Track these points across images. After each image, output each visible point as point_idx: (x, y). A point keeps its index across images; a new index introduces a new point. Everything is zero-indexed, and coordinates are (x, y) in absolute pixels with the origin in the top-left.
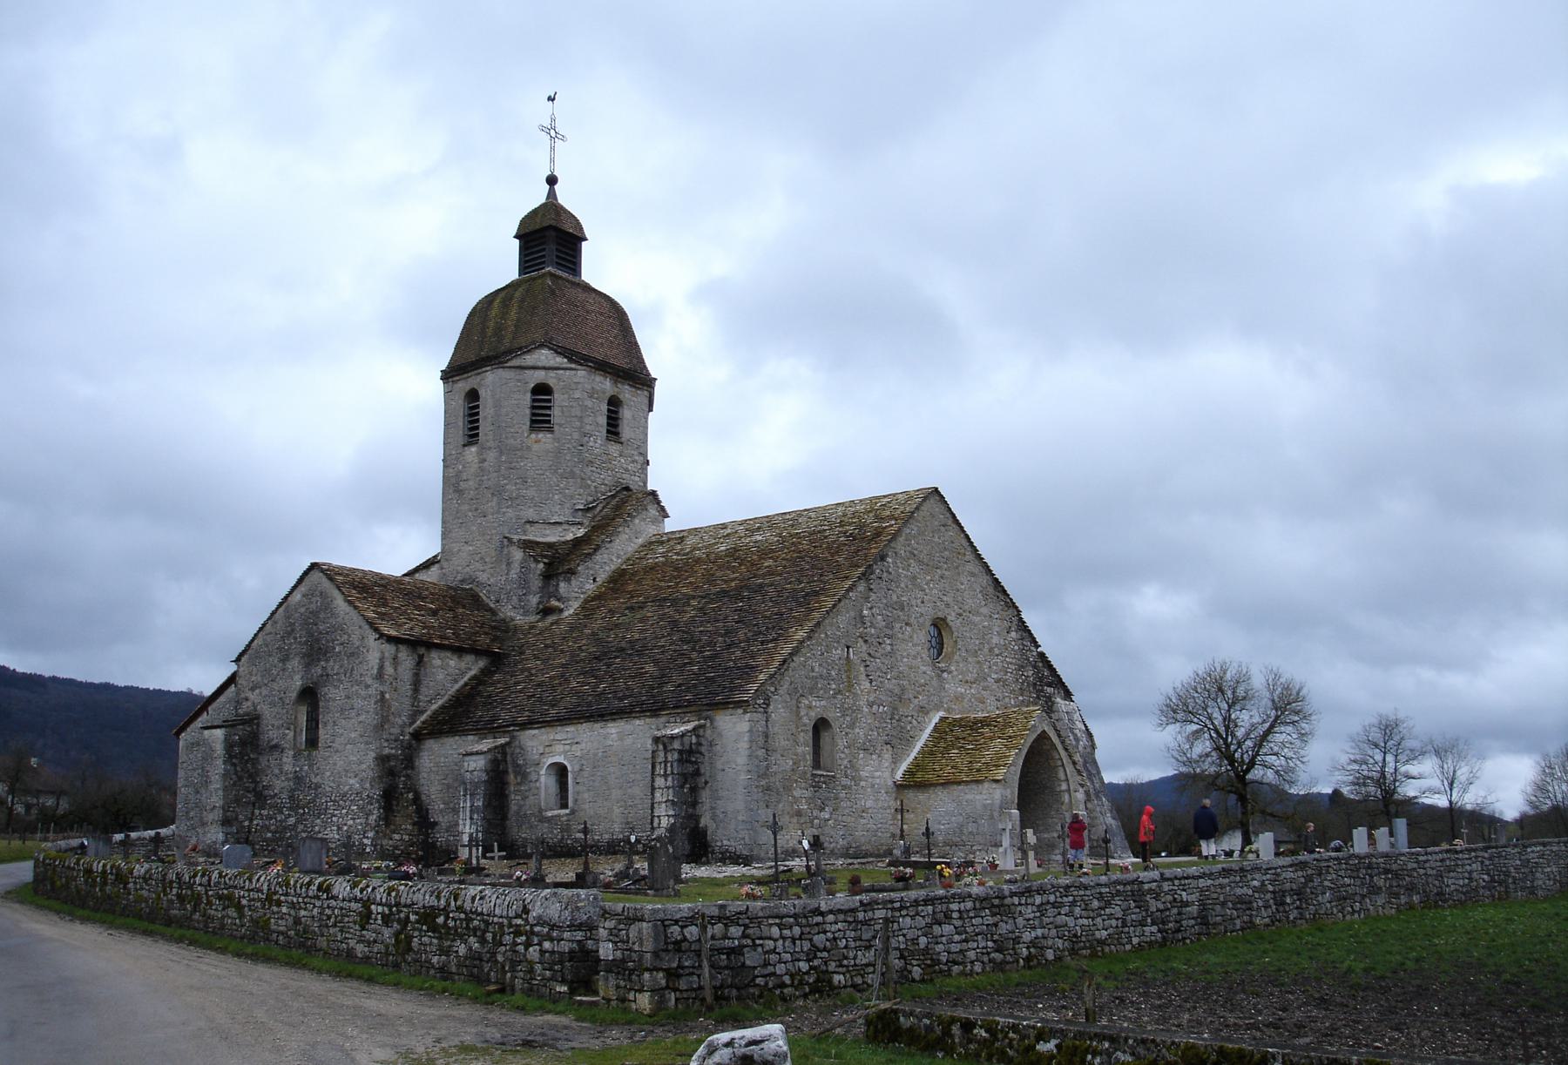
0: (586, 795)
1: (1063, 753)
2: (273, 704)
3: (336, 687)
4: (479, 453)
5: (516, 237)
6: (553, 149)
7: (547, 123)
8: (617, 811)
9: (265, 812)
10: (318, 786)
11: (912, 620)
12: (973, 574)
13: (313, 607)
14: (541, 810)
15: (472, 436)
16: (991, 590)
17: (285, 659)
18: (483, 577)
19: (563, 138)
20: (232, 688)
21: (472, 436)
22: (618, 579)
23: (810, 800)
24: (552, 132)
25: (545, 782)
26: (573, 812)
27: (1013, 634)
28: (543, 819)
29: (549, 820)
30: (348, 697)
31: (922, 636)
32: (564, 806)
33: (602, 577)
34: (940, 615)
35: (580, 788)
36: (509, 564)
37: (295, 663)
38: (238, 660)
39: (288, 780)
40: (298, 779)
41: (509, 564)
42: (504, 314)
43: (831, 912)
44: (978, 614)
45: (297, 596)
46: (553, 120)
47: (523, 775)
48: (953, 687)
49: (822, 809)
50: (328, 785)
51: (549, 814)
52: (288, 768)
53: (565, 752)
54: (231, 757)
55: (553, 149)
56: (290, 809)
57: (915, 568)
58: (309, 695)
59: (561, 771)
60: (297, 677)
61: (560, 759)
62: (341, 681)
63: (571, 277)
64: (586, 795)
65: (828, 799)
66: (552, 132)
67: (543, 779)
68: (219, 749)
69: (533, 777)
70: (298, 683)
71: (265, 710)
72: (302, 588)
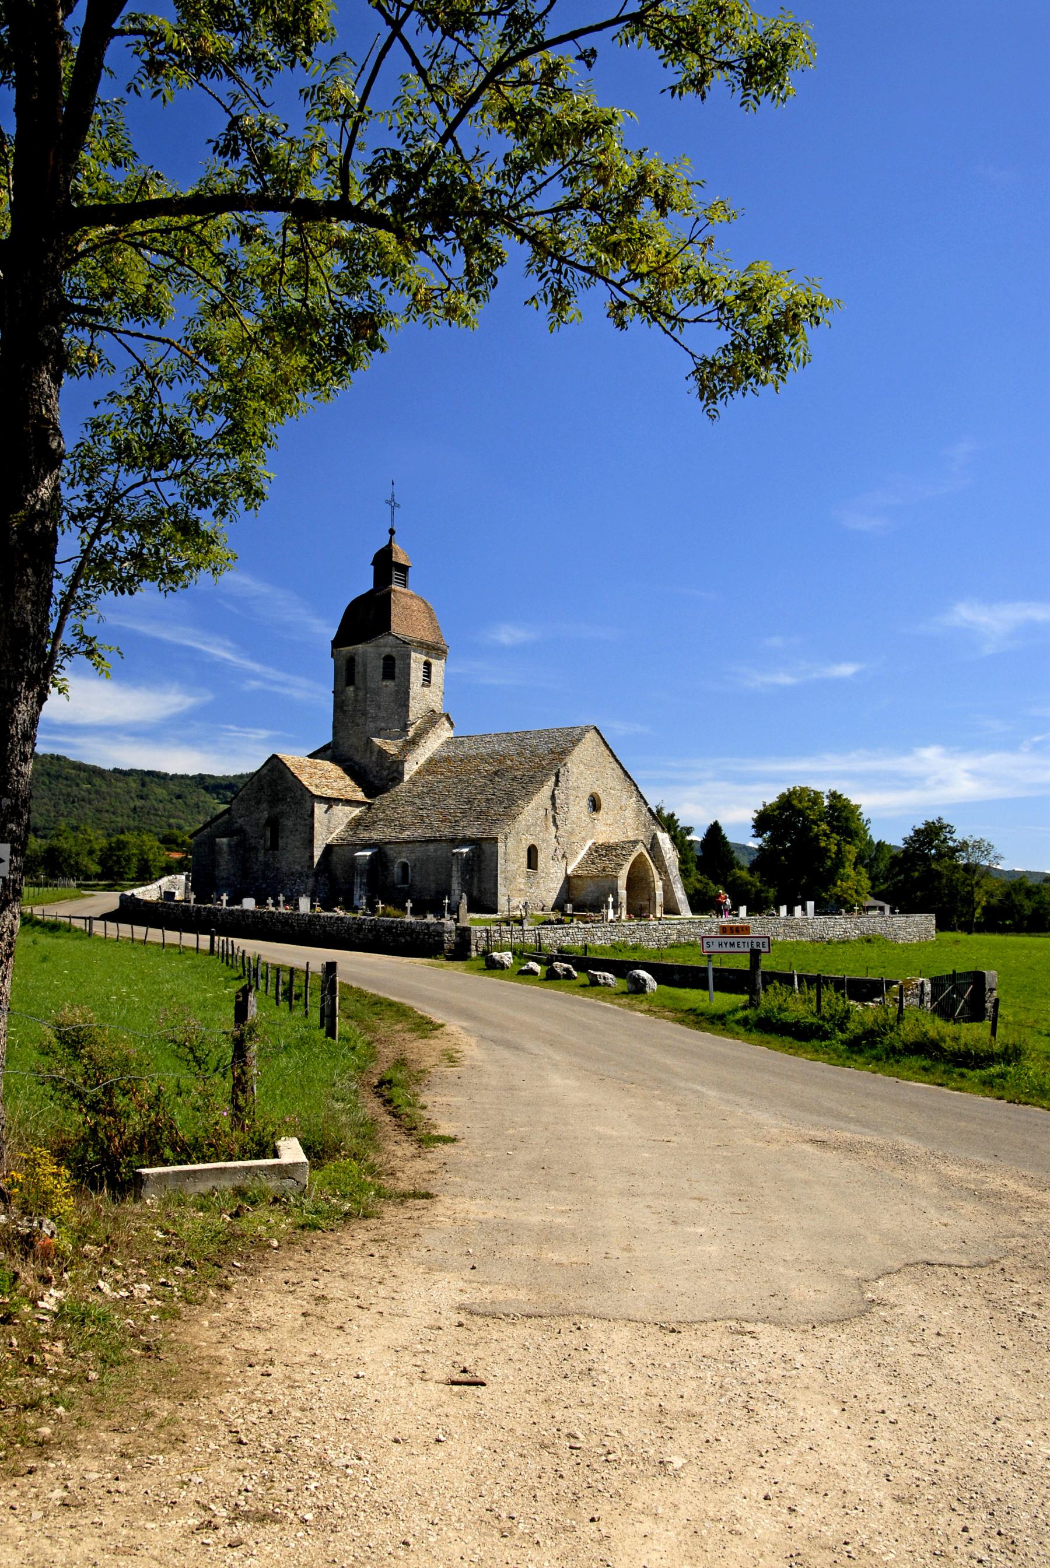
4: (355, 691)
6: (393, 513)
7: (389, 499)
8: (433, 886)
10: (278, 869)
14: (394, 885)
15: (350, 680)
16: (623, 776)
17: (258, 803)
18: (357, 758)
19: (399, 506)
20: (227, 816)
21: (350, 680)
22: (430, 761)
23: (525, 884)
24: (393, 504)
25: (396, 870)
26: (411, 885)
31: (585, 802)
33: (422, 761)
36: (371, 753)
37: (265, 805)
40: (266, 864)
41: (371, 753)
43: (901, 1010)
46: (393, 496)
48: (600, 827)
50: (285, 869)
55: (393, 513)
57: (582, 767)
58: (274, 824)
61: (403, 860)
63: (493, 916)
66: (393, 504)
68: (225, 848)
71: (247, 828)
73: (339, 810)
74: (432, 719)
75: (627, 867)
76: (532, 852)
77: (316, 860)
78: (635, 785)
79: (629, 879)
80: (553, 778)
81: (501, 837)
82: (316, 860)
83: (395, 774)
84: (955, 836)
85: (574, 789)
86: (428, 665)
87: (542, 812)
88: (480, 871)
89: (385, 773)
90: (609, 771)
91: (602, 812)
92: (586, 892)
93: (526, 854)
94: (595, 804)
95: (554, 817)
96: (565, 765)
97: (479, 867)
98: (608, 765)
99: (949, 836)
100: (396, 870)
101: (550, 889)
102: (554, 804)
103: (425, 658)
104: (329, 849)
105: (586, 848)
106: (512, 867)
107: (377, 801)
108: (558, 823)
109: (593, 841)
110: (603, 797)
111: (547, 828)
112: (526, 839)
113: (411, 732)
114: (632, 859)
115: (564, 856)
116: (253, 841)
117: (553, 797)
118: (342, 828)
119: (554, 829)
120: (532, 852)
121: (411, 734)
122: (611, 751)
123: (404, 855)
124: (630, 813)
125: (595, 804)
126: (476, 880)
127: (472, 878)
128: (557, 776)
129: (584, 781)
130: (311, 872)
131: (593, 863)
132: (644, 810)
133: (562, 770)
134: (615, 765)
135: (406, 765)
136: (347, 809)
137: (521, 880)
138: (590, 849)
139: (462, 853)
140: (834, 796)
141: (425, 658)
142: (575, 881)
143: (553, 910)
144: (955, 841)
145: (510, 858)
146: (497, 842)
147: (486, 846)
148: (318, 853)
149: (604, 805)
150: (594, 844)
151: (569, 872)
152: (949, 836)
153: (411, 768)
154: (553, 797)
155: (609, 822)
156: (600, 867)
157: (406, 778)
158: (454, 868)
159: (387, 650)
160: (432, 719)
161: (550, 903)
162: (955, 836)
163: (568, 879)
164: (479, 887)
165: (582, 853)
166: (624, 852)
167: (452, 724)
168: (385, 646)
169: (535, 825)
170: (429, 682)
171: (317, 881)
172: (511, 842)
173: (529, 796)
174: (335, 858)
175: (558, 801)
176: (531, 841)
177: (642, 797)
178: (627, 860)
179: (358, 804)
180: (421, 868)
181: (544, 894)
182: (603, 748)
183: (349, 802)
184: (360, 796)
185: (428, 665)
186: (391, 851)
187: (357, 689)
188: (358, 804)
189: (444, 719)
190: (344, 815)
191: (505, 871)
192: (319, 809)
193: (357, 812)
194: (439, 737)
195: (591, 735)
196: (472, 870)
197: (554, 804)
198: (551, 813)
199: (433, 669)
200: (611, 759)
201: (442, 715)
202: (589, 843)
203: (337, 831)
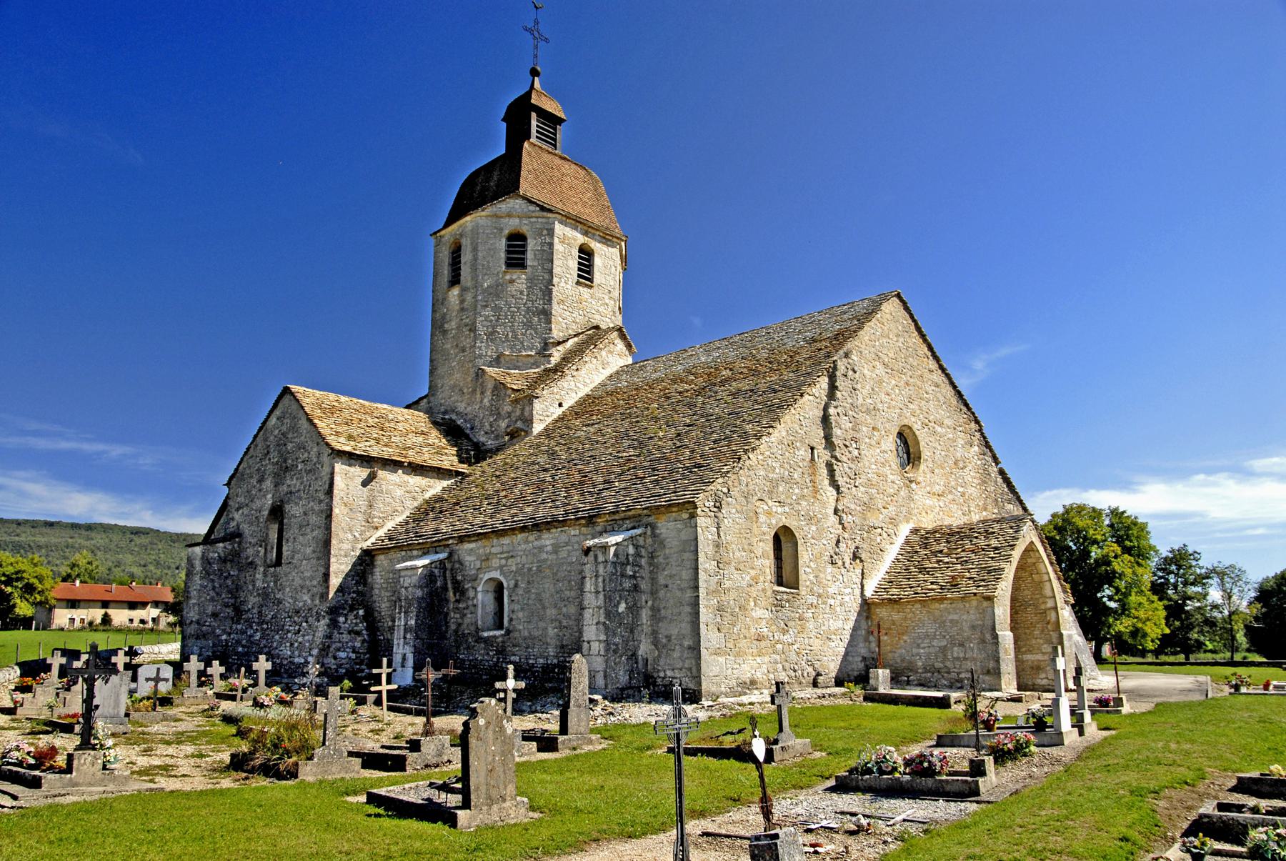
0: (521, 615)
1: (57, 799)
2: (251, 523)
3: (297, 504)
4: (461, 295)
5: (503, 120)
8: (552, 632)
9: (239, 627)
11: (879, 426)
12: (937, 386)
13: (284, 428)
14: (477, 630)
16: (954, 401)
17: (261, 481)
18: (461, 407)
23: (770, 622)
25: (482, 598)
26: (508, 632)
27: (976, 448)
28: (479, 640)
29: (487, 641)
30: (305, 514)
32: (500, 627)
34: (906, 422)
35: (516, 607)
38: (228, 484)
39: (259, 595)
40: (265, 594)
42: (488, 180)
44: (941, 425)
45: (273, 420)
47: (459, 589)
48: (921, 497)
49: (785, 632)
51: (485, 634)
52: (259, 584)
53: (501, 567)
54: (208, 574)
56: (258, 624)
57: (880, 370)
59: (499, 589)
60: (269, 496)
61: (496, 574)
62: (300, 498)
64: (521, 615)
65: (792, 619)
67: (480, 596)
69: (471, 593)
70: (269, 501)
72: (277, 412)
73: (390, 480)
74: (593, 336)
75: (1009, 572)
76: (783, 541)
77: (335, 582)
78: (977, 422)
79: (1014, 599)
80: (824, 382)
81: (704, 501)
82: (335, 582)
83: (519, 424)
84: (1201, 563)
85: (868, 412)
86: (586, 255)
87: (803, 453)
88: (654, 593)
89: (503, 424)
90: (930, 389)
91: (923, 467)
92: (915, 639)
93: (769, 547)
94: (909, 451)
95: (829, 466)
96: (847, 355)
97: (653, 580)
98: (927, 375)
99: (1194, 563)
100: (482, 598)
101: (828, 634)
102: (828, 438)
103: (581, 239)
104: (367, 558)
105: (900, 540)
106: (736, 579)
107: (477, 470)
108: (841, 481)
109: (911, 525)
110: (922, 435)
111: (816, 491)
112: (769, 513)
113: (556, 355)
114: (1017, 554)
115: (855, 557)
116: (250, 551)
117: (825, 419)
118: (401, 518)
119: (832, 492)
120: (783, 541)
121: (555, 359)
122: (930, 348)
123: (495, 562)
124: (970, 475)
125: (909, 451)
126: (645, 615)
127: (634, 609)
128: (832, 378)
129: (886, 399)
130: (324, 607)
131: (923, 570)
132: (994, 470)
133: (841, 366)
134: (938, 377)
135: (538, 405)
136: (415, 481)
137: (760, 613)
138: (907, 542)
139: (605, 548)
140: (1115, 513)
141: (581, 239)
142: (882, 613)
143: (839, 682)
144: (1201, 568)
145: (729, 541)
146: (693, 516)
147: (667, 527)
148: (340, 567)
149: (926, 454)
150: (915, 531)
151: (869, 593)
152: (1194, 563)
153: (545, 412)
154: (825, 419)
155: (937, 489)
156: (943, 577)
157: (538, 428)
158: (589, 586)
159: (512, 225)
160: (593, 336)
161: (831, 667)
162: (1201, 563)
163: (867, 606)
164: (654, 633)
165: (893, 551)
166: (994, 542)
167: (629, 346)
168: (509, 215)
169: (790, 480)
170: (591, 280)
171: (334, 624)
172: (732, 515)
173: (773, 411)
174: (378, 577)
175: (837, 432)
176: (781, 517)
177: (988, 446)
178: (1007, 559)
179: (440, 473)
180: (528, 591)
181: (817, 643)
182: (915, 339)
183: (417, 469)
184: (449, 460)
185: (586, 255)
186: (469, 553)
187: (464, 290)
188: (440, 473)
189: (616, 334)
190: (403, 494)
191: (719, 589)
192: (347, 478)
193: (437, 487)
194: (605, 365)
195: (891, 308)
196: (636, 588)
197: (828, 438)
198: (823, 455)
199: (598, 261)
200: (932, 365)
201: (610, 330)
202: (904, 530)
203: (390, 525)
